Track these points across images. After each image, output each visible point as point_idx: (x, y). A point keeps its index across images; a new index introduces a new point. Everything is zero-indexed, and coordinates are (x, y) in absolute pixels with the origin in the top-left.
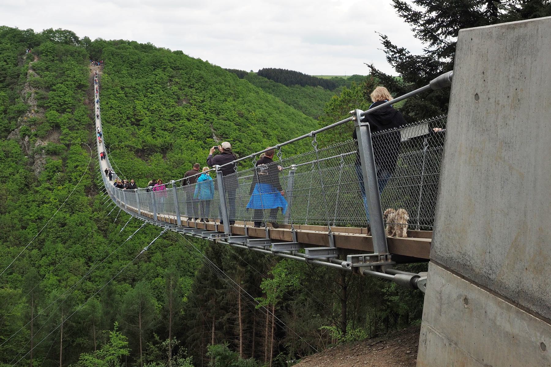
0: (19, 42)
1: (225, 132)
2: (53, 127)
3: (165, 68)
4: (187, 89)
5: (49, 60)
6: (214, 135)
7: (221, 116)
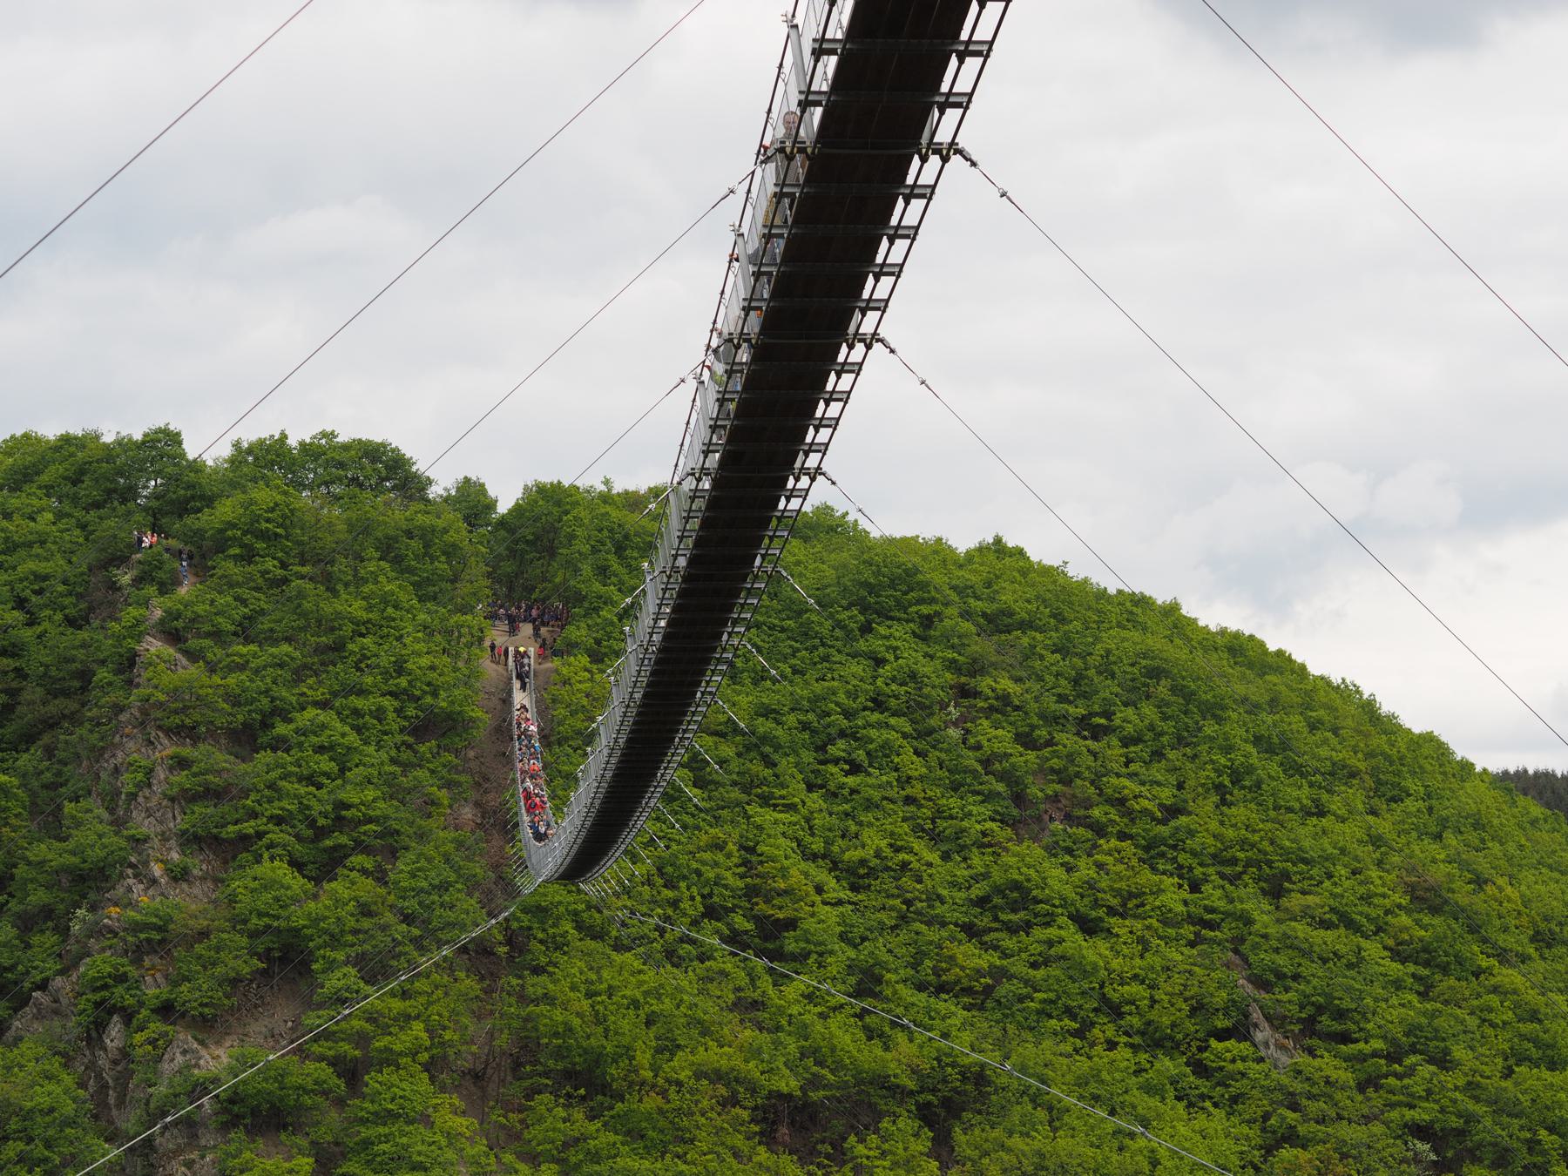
0: (97, 505)
1: (1330, 997)
2: (266, 956)
3: (928, 621)
4: (1067, 740)
5: (260, 581)
6: (1256, 1015)
7: (1295, 901)
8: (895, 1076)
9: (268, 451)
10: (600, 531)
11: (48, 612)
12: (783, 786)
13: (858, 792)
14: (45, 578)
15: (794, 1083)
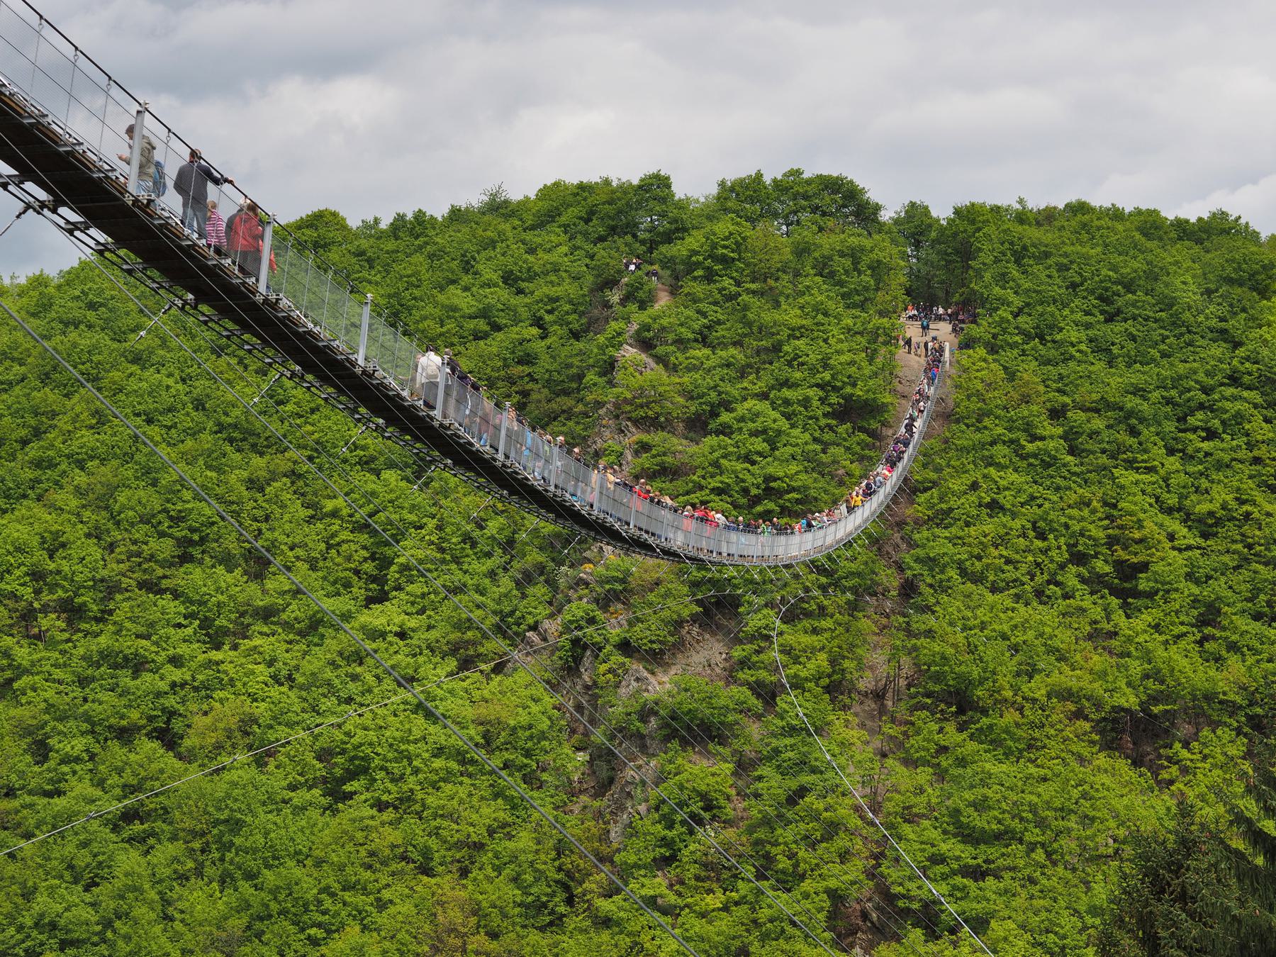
8: (1225, 693)
9: (747, 188)
10: (1002, 244)
11: (556, 327)
12: (1146, 451)
13: (1211, 455)
14: (557, 299)
15: (1133, 699)
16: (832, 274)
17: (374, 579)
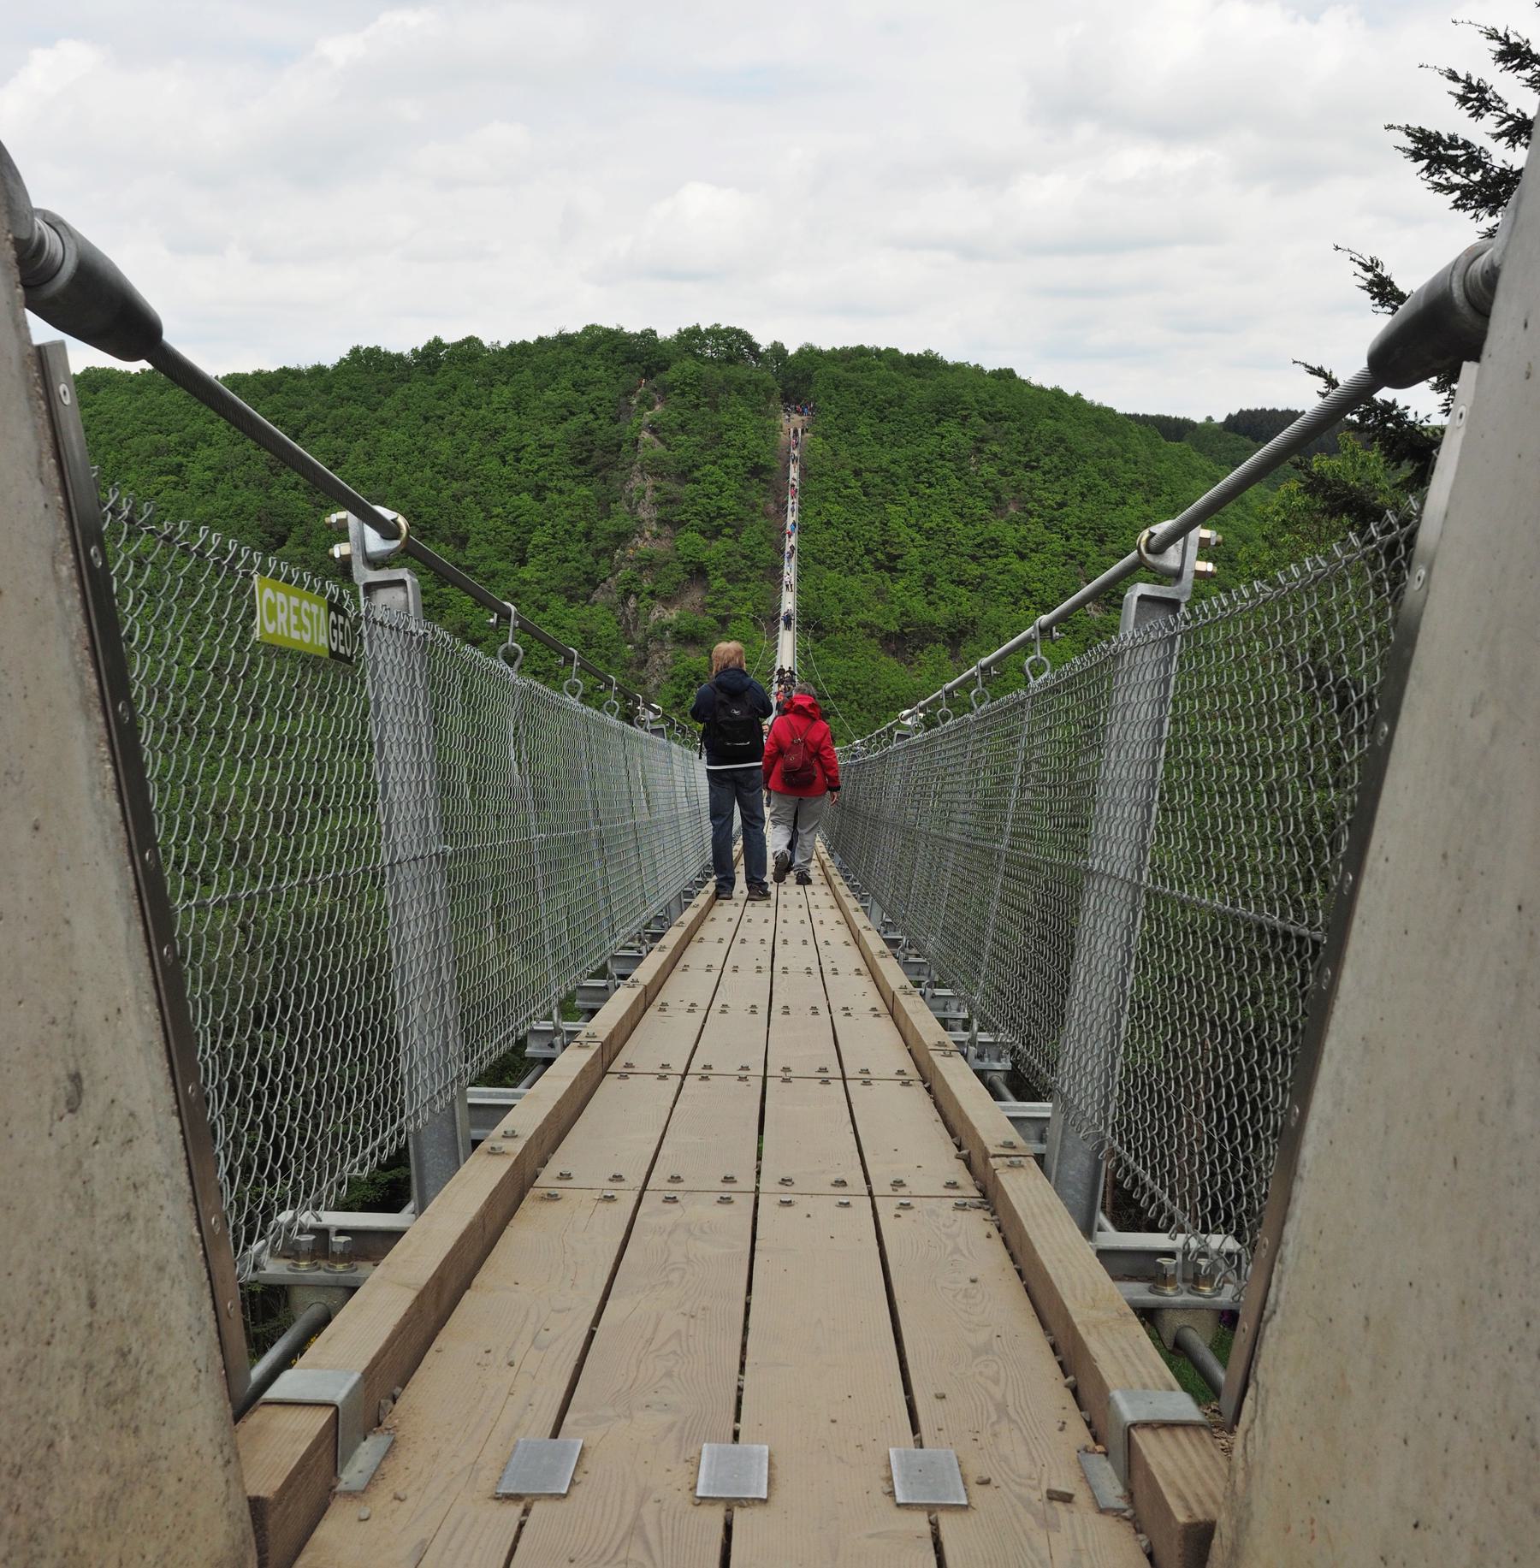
16: (745, 394)
17: (519, 550)
